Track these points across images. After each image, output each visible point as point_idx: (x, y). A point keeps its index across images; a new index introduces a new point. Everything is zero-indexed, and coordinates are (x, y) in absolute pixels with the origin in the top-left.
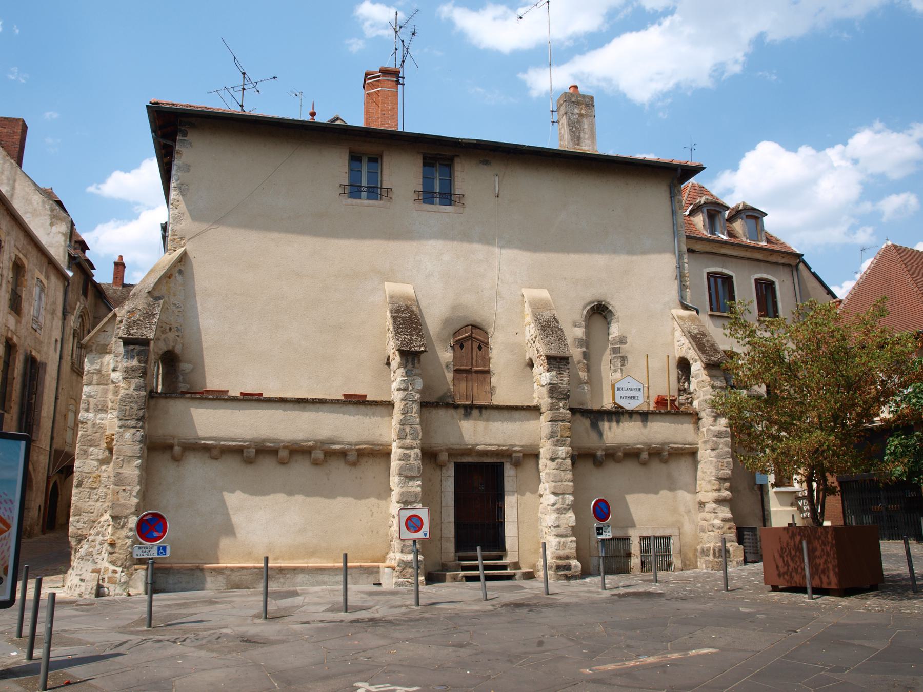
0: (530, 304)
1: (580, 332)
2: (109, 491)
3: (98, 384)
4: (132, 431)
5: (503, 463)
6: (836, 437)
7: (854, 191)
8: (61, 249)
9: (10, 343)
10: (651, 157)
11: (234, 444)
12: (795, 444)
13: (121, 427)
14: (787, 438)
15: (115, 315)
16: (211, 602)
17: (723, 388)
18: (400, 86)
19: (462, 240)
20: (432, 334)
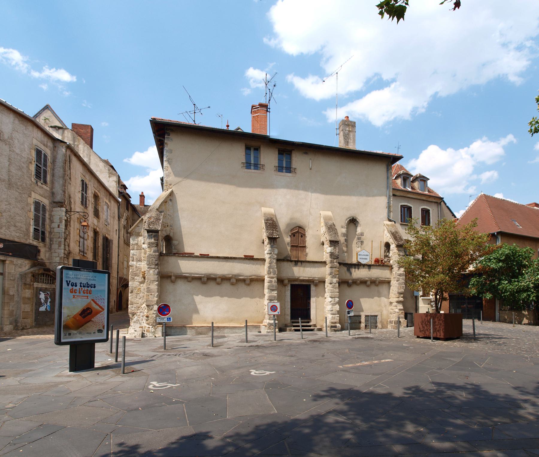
0: (323, 217)
1: (344, 230)
2: (145, 295)
3: (137, 250)
4: (153, 270)
5: (310, 285)
7: (470, 170)
8: (115, 188)
10: (380, 152)
11: (197, 275)
13: (148, 268)
14: (428, 277)
15: (142, 219)
16: (190, 340)
17: (403, 256)
18: (268, 113)
19: (295, 189)
20: (281, 230)
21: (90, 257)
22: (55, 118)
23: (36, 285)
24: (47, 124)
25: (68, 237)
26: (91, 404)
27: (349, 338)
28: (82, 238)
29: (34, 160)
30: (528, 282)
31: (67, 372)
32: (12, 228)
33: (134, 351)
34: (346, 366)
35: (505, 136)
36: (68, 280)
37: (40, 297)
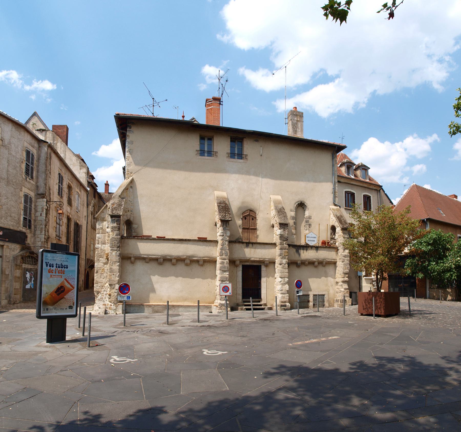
0: (273, 201)
1: (293, 214)
2: (108, 275)
3: (102, 233)
4: (116, 251)
6: (388, 259)
7: (404, 162)
8: (85, 179)
9: (69, 218)
10: (325, 141)
11: (154, 257)
12: (372, 261)
13: (111, 250)
14: (370, 258)
15: (107, 206)
16: (147, 318)
17: (348, 238)
18: (221, 106)
19: (246, 174)
20: (234, 213)
21: (64, 241)
22: (40, 122)
23: (24, 266)
24: (34, 128)
25: (48, 224)
26: (62, 373)
27: (298, 317)
28: (58, 224)
29: (24, 160)
30: (451, 264)
31: (45, 343)
32: (9, 218)
33: (98, 327)
34: (296, 343)
35: (431, 135)
36: (47, 261)
37: (27, 276)
